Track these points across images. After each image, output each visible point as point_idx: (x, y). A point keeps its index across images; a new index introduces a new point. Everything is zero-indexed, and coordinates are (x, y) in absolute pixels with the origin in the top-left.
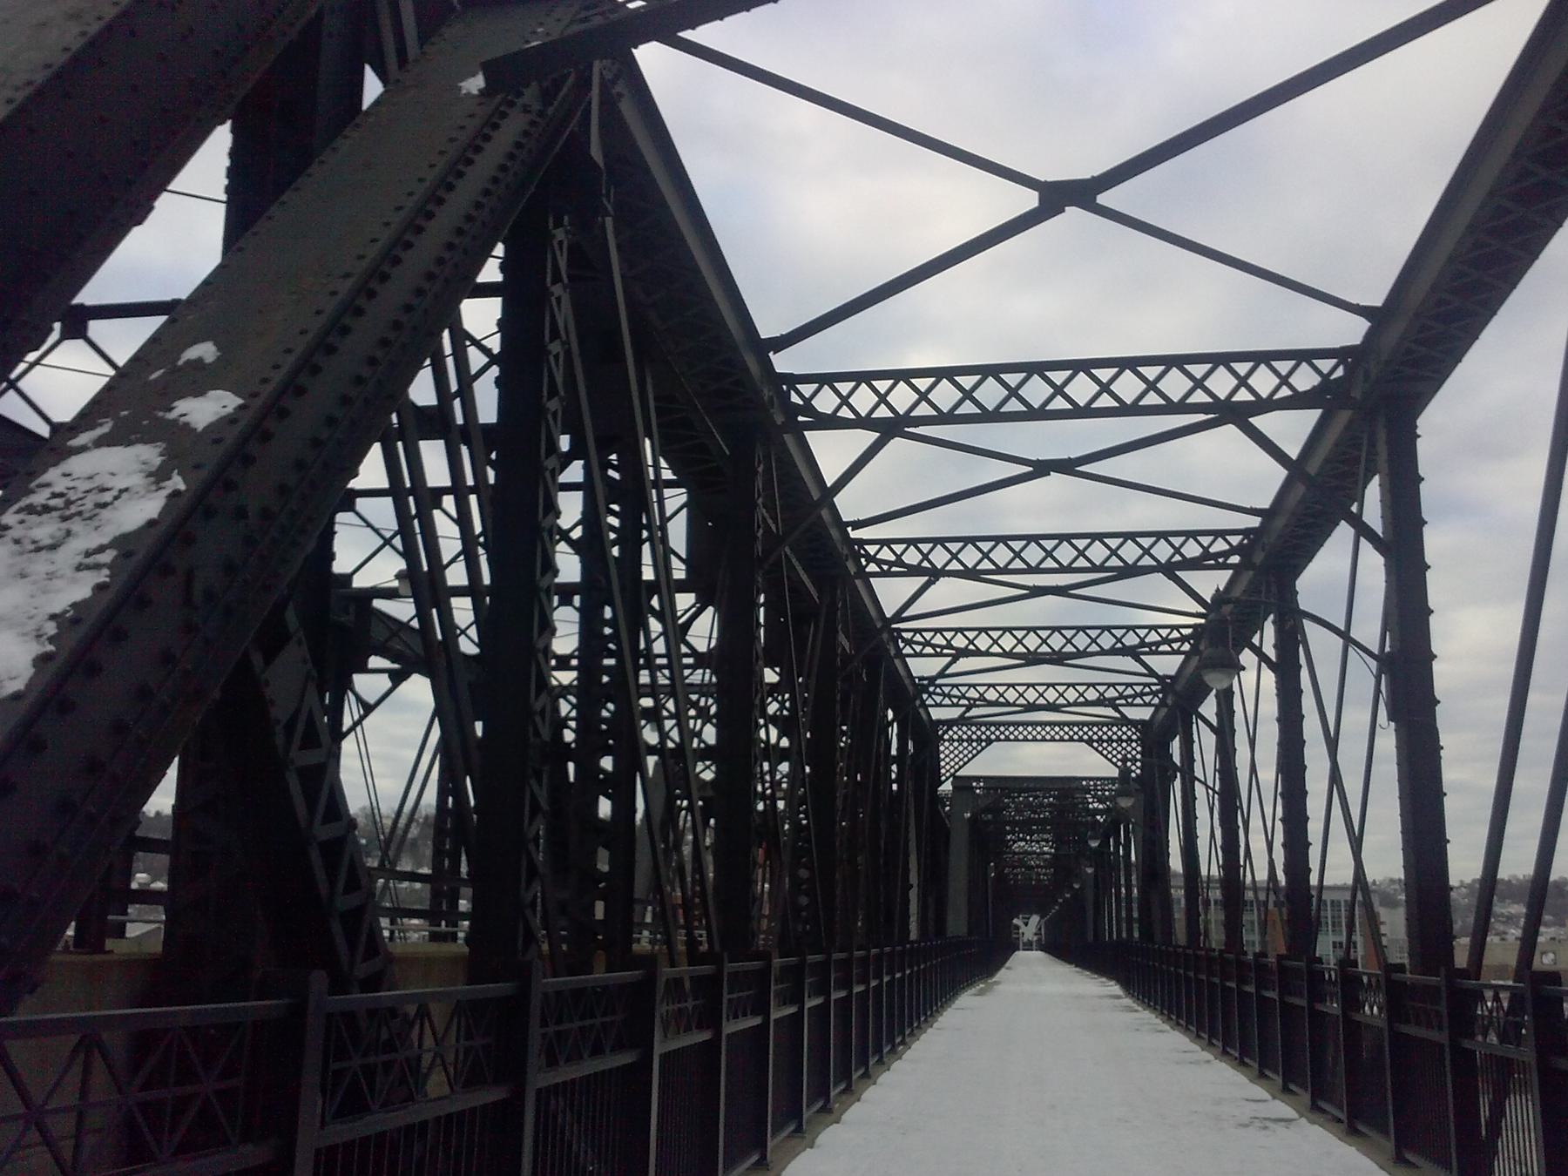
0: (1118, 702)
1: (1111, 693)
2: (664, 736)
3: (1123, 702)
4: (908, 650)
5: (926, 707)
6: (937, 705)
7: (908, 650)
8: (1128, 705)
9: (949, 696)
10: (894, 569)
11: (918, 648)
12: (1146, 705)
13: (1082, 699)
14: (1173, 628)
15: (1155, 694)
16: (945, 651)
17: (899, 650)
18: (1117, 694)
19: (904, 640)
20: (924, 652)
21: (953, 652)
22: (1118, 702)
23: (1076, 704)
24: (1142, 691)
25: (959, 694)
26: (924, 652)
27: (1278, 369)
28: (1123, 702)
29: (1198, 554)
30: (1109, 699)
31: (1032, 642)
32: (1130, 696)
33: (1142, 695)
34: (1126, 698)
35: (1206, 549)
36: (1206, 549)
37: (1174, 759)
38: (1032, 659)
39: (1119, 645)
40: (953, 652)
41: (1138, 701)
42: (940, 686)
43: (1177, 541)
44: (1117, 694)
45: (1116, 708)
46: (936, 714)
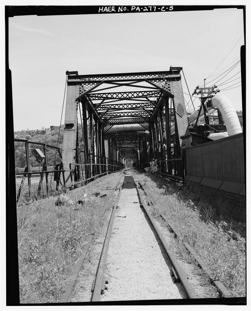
0: (148, 96)
1: (146, 94)
2: (102, 120)
3: (149, 96)
4: (92, 99)
5: (91, 101)
6: (94, 100)
7: (92, 99)
8: (150, 97)
9: (98, 97)
10: (92, 95)
11: (94, 98)
12: (156, 96)
13: (123, 108)
14: (150, 91)
15: (158, 93)
16: (101, 98)
17: (89, 99)
18: (147, 94)
19: (91, 96)
20: (96, 99)
21: (103, 98)
22: (148, 96)
23: (137, 97)
24: (154, 93)
25: (100, 96)
26: (96, 99)
27: (68, 181)
28: (149, 96)
29: (141, 95)
30: (145, 96)
31: (120, 96)
32: (143, 106)
33: (154, 94)
34: (150, 95)
35: (143, 94)
36: (143, 94)
37: (39, 149)
38: (121, 99)
39: (138, 96)
40: (103, 98)
41: (153, 96)
42: (107, 113)
43: (138, 93)
44: (147, 94)
45: (147, 98)
46: (94, 102)
